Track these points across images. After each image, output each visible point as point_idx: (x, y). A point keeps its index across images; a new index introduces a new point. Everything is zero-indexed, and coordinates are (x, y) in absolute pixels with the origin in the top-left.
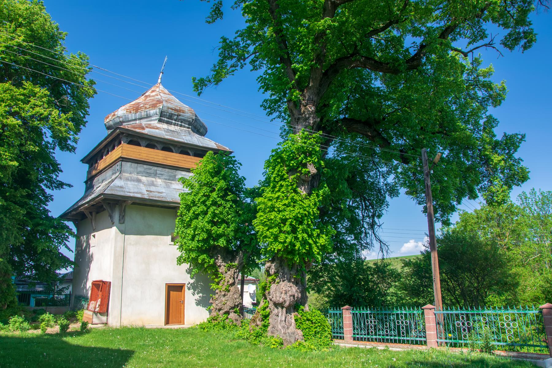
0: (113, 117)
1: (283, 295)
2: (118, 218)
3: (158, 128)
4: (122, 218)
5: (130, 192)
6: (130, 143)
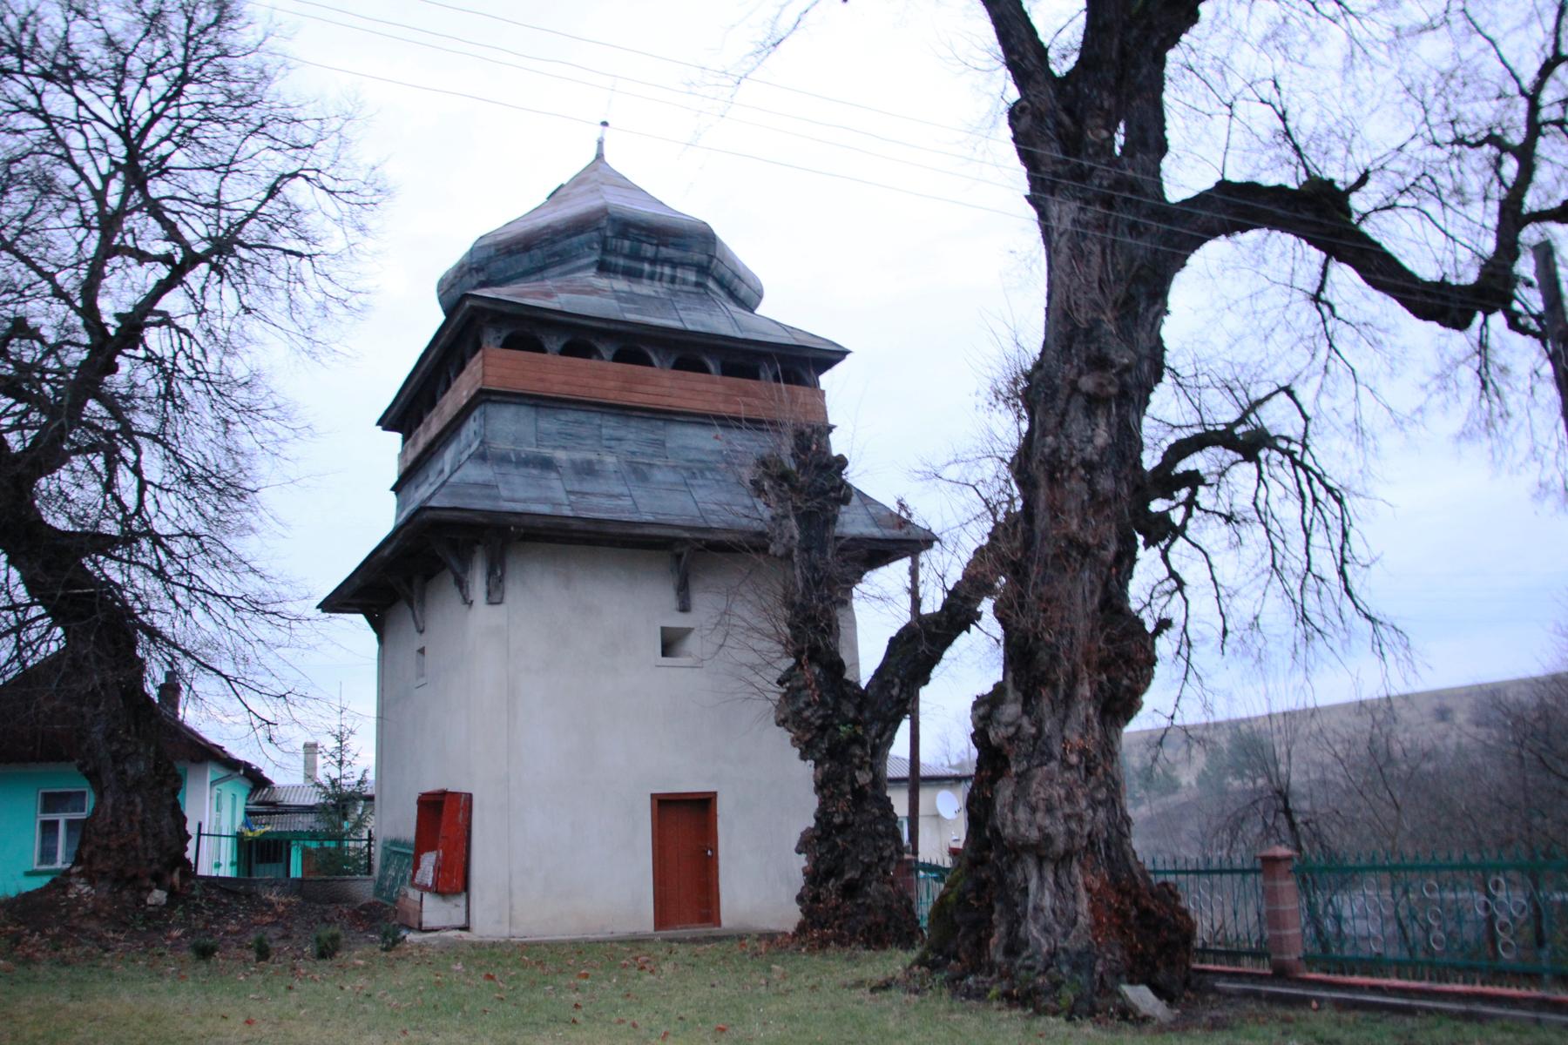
1: (1039, 816)
3: (595, 291)
5: (513, 500)
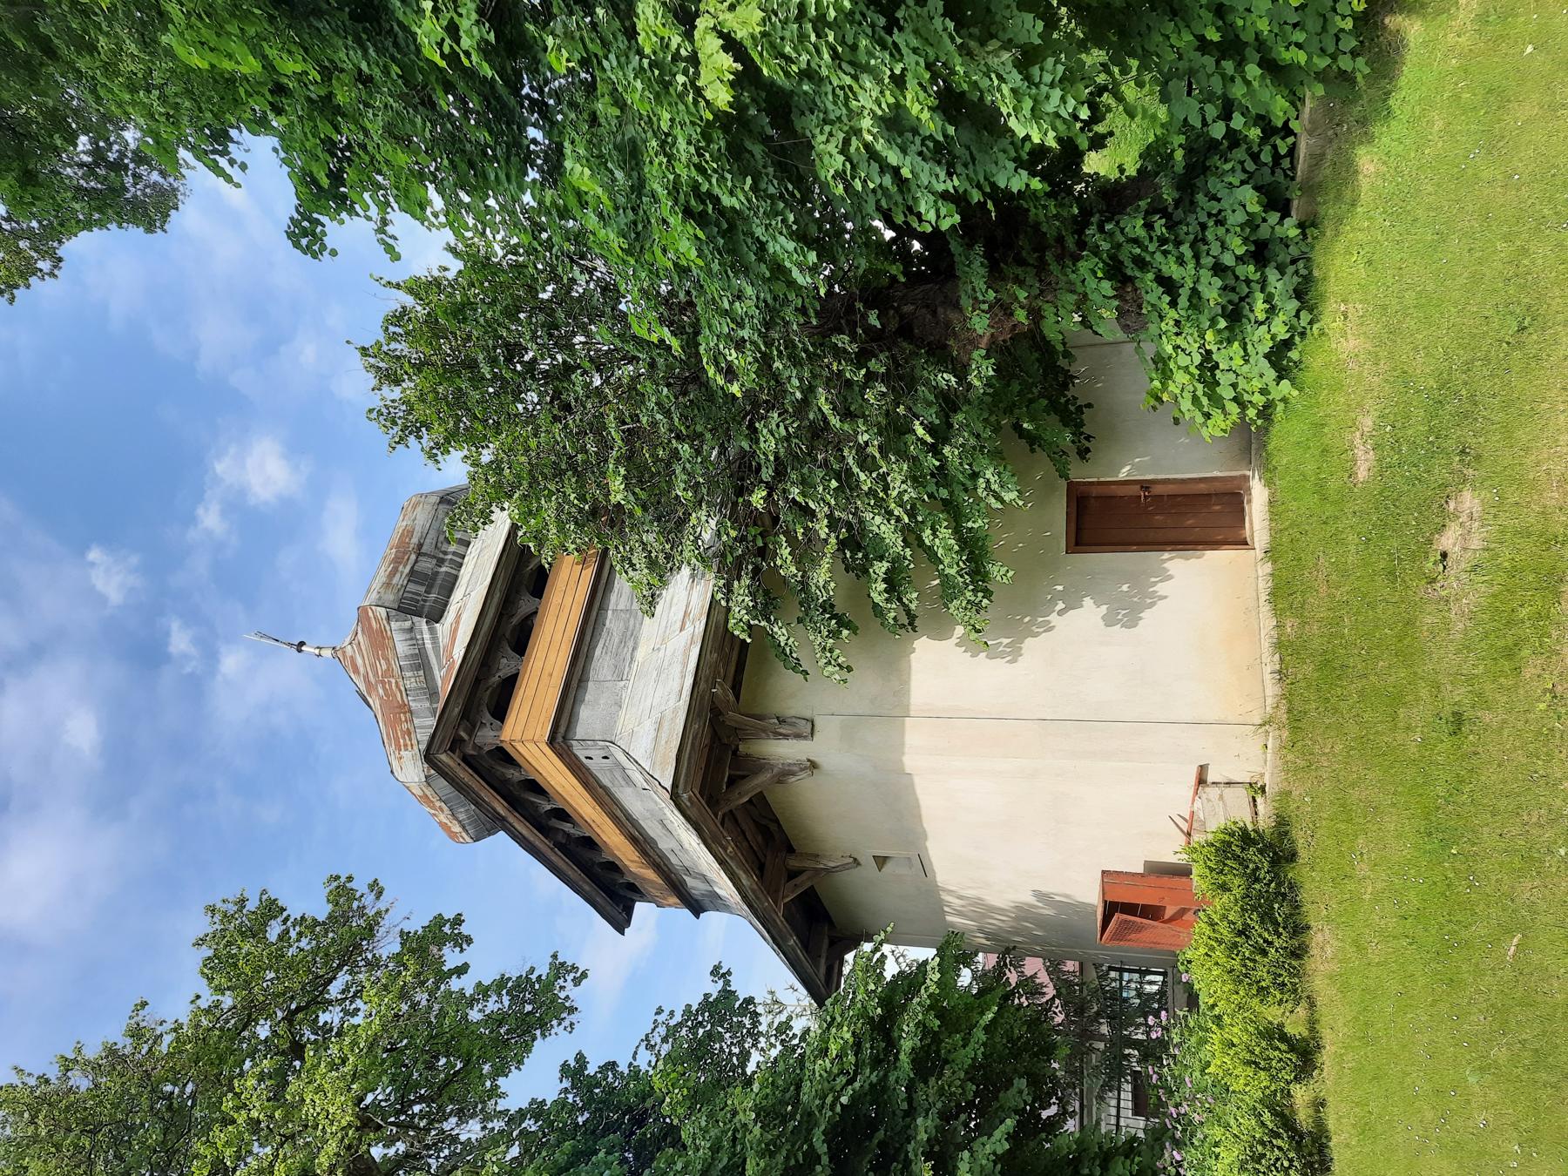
0: (438, 804)
2: (792, 742)
4: (793, 725)
6: (500, 712)
